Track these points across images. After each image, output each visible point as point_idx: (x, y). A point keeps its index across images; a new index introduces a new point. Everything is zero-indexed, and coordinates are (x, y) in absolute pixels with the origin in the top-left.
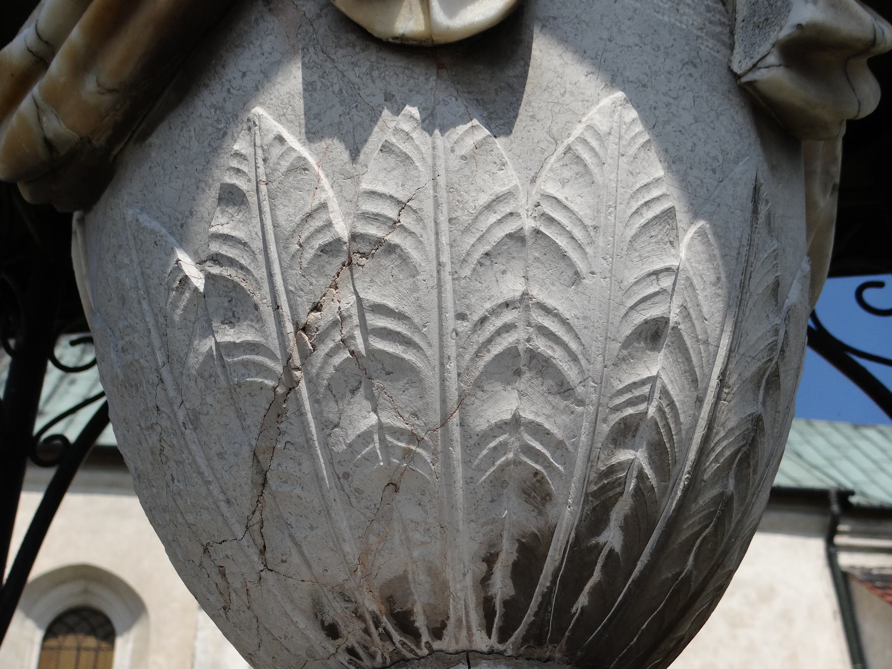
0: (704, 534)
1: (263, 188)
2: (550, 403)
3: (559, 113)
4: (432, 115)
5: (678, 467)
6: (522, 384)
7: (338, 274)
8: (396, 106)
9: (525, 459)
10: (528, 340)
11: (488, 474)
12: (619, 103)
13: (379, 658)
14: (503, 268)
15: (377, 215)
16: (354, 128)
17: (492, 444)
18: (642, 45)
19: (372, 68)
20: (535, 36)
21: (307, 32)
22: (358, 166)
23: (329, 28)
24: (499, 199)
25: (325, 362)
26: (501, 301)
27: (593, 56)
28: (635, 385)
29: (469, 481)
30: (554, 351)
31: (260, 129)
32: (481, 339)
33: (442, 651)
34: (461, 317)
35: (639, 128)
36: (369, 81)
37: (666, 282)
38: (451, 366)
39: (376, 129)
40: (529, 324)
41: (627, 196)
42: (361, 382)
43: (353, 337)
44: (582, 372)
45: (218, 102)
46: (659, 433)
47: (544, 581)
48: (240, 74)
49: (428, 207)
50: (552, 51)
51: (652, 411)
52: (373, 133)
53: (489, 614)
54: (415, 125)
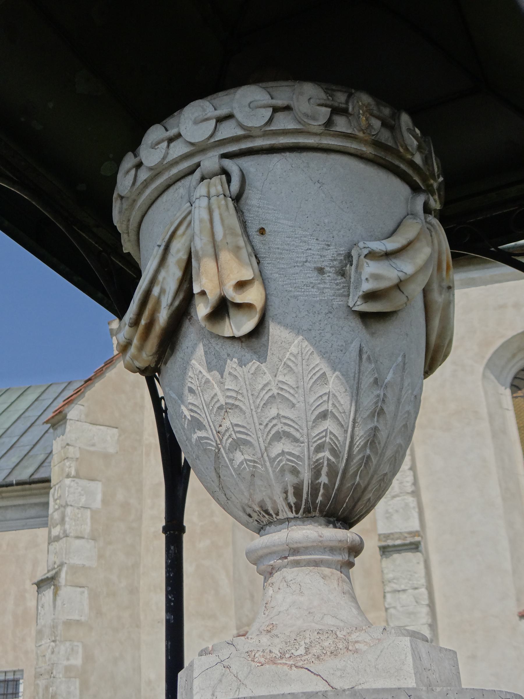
0: (361, 469)
1: (199, 388)
2: (293, 445)
5: (342, 453)
6: (283, 441)
7: (224, 415)
9: (288, 463)
10: (282, 428)
11: (278, 469)
13: (264, 522)
14: (270, 407)
15: (231, 396)
17: (278, 460)
19: (222, 345)
22: (224, 379)
24: (265, 385)
25: (226, 442)
26: (271, 418)
27: (291, 325)
28: (320, 433)
29: (274, 471)
30: (290, 429)
33: (280, 519)
34: (260, 424)
37: (325, 398)
38: (261, 440)
40: (281, 423)
41: (307, 373)
42: (237, 447)
43: (231, 434)
44: (301, 433)
46: (332, 446)
47: (305, 496)
49: (245, 392)
51: (328, 440)
53: (290, 507)
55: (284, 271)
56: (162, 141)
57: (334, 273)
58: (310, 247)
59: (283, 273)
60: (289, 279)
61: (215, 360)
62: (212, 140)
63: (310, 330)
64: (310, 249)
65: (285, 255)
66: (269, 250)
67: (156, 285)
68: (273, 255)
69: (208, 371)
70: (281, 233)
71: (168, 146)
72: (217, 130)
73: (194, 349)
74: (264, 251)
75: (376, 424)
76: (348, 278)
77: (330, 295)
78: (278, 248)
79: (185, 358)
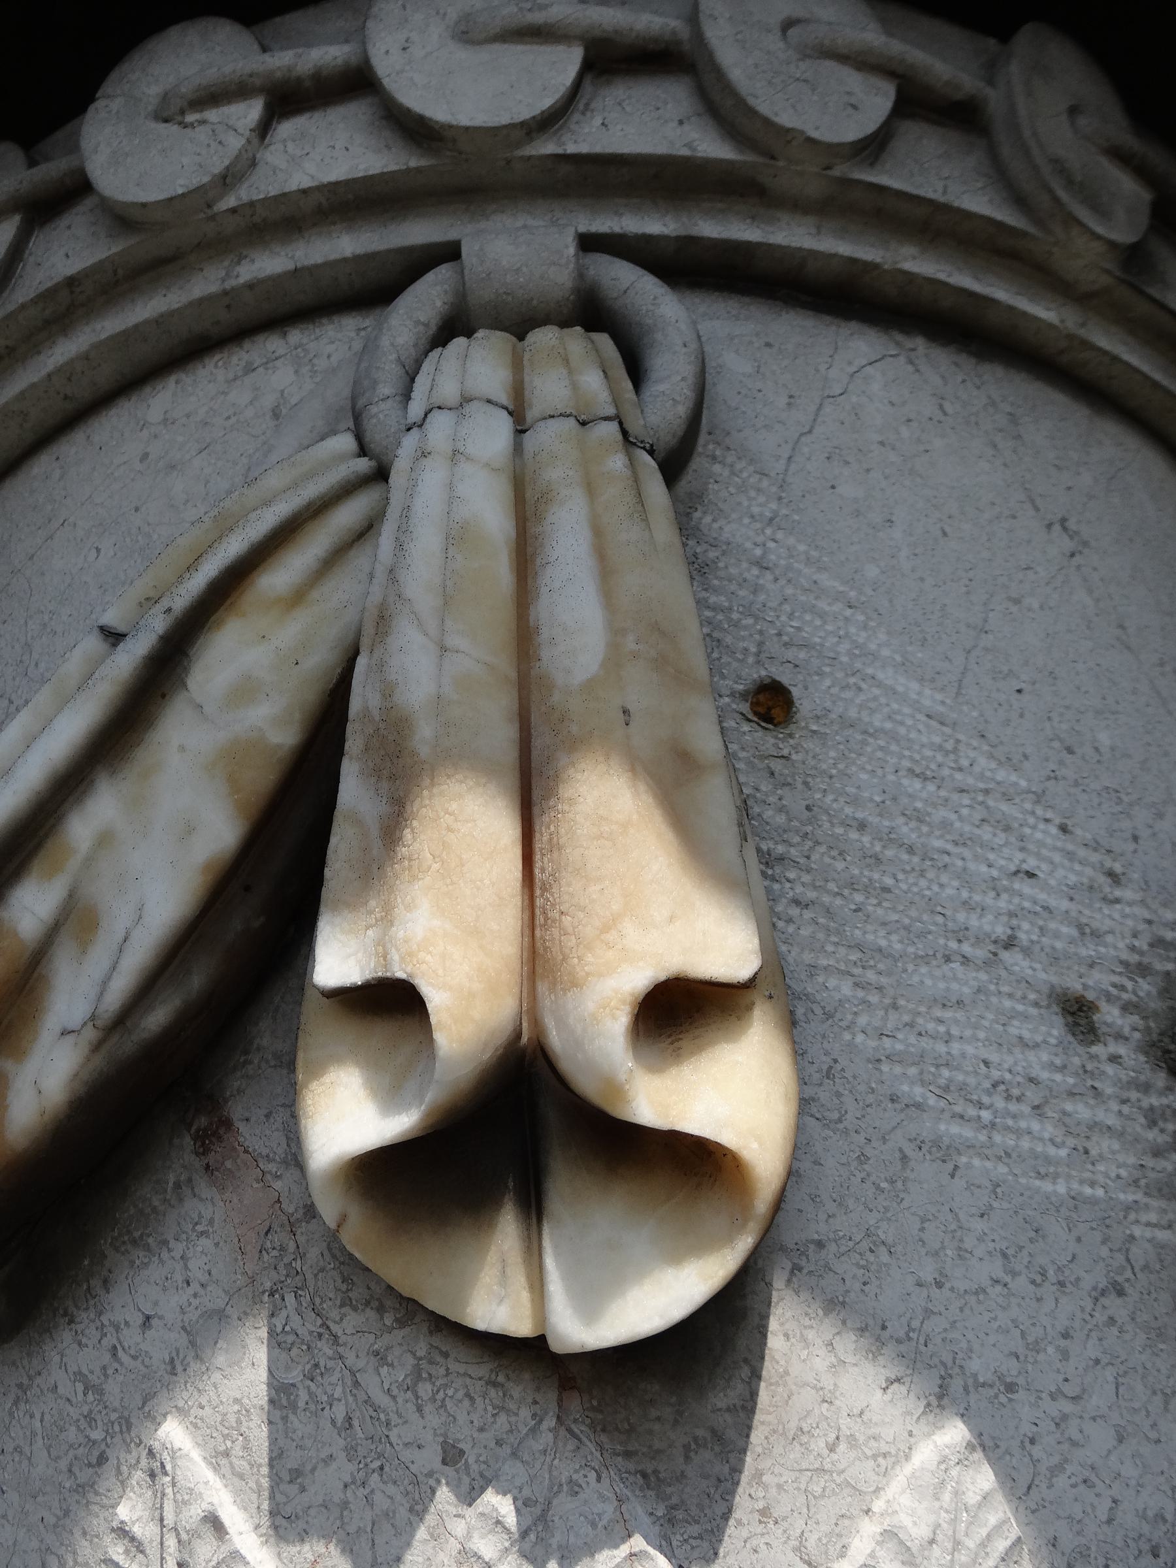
3: (823, 1496)
4: (543, 1518)
8: (466, 1480)
12: (954, 1459)
16: (373, 1524)
18: (1008, 1279)
19: (417, 1375)
20: (775, 1296)
21: (283, 1249)
23: (329, 1249)
27: (901, 1334)
31: (174, 1485)
35: (999, 1512)
36: (411, 1407)
39: (422, 1533)
45: (92, 1372)
48: (140, 1320)
50: (811, 1335)
52: (415, 1543)
54: (507, 1544)
55: (889, 974)
56: (235, 91)
58: (1031, 864)
59: (884, 980)
60: (911, 1025)
61: (344, 1469)
62: (547, 147)
63: (1011, 1388)
64: (1031, 875)
65: (901, 876)
66: (810, 822)
67: (37, 866)
68: (827, 860)
69: (276, 1528)
70: (882, 743)
71: (264, 129)
72: (581, 106)
73: (193, 1344)
74: (781, 819)
77: (1118, 1177)
78: (862, 826)
79: (112, 1388)
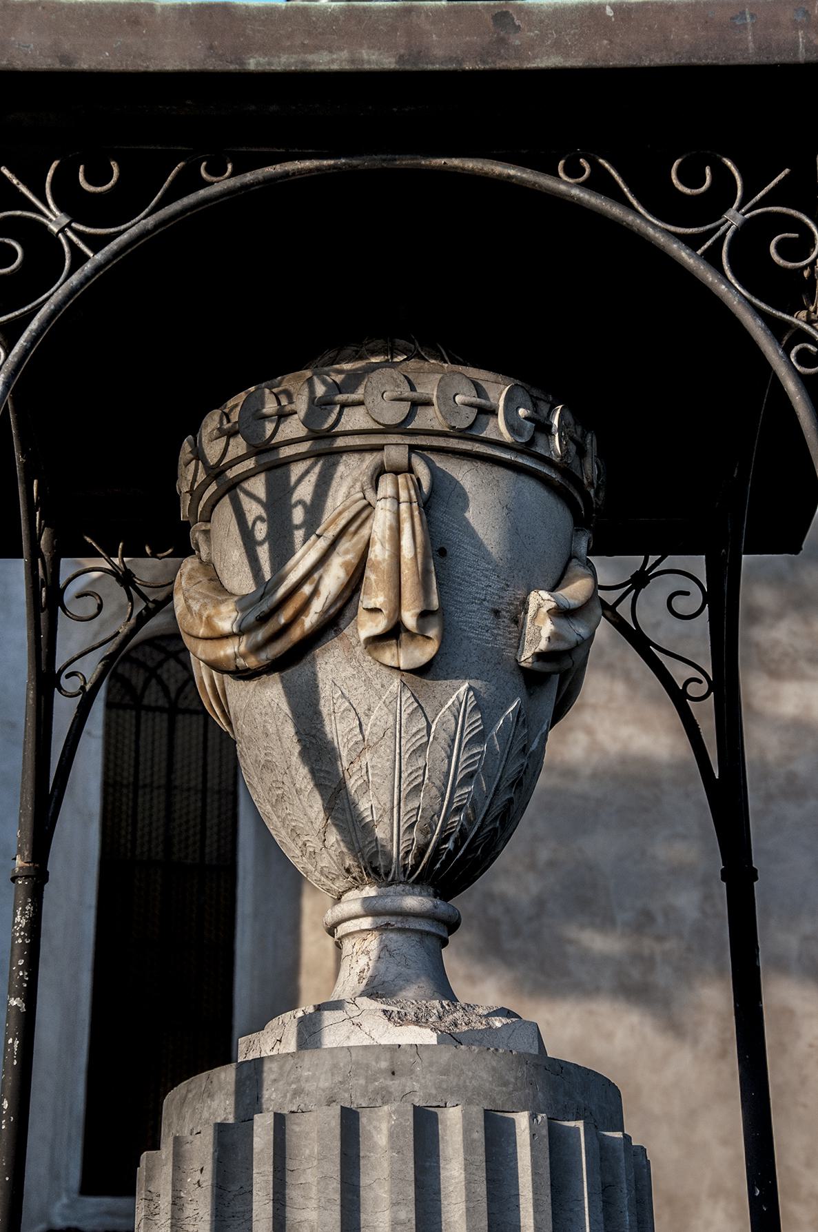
32: (410, 780)
57: (509, 619)
75: (512, 795)
76: (520, 628)
